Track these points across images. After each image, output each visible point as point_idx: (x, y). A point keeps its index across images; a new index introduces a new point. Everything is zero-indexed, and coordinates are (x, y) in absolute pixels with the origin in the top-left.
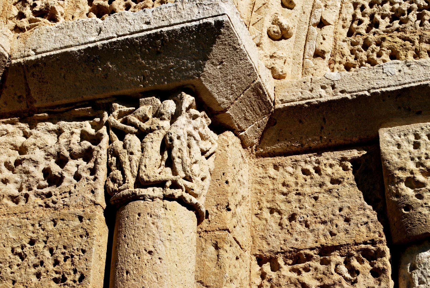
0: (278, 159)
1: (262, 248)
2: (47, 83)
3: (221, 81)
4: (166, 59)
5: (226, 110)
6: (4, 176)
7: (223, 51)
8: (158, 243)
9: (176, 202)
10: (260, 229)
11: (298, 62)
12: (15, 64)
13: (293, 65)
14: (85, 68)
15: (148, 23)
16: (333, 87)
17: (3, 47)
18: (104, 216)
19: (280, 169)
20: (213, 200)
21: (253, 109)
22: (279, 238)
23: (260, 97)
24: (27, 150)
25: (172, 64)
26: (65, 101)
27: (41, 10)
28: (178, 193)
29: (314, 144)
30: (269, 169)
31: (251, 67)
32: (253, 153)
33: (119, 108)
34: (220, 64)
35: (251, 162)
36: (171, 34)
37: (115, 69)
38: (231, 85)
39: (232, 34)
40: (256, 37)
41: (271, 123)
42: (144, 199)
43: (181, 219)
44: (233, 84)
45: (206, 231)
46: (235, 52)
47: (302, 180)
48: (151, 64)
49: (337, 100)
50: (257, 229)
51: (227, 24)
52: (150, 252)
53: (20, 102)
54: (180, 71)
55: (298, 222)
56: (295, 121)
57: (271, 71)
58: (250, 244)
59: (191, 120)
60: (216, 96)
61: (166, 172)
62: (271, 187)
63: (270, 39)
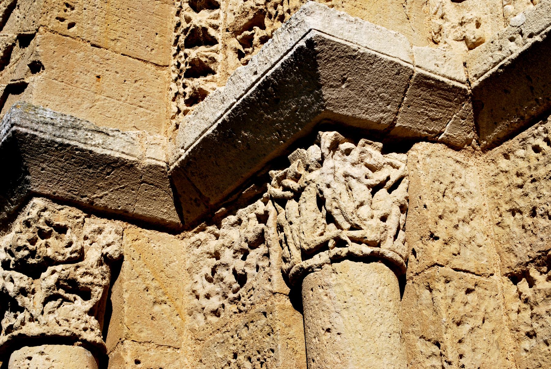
0: (505, 146)
1: (510, 264)
2: (208, 177)
3: (360, 99)
4: (287, 104)
5: (392, 124)
6: (206, 291)
7: (336, 67)
8: (334, 317)
9: (348, 261)
10: (505, 241)
11: (496, 15)
12: (173, 170)
13: (492, 21)
14: (227, 146)
15: (256, 73)
16: (521, 33)
17: (154, 159)
18: (291, 303)
19: (511, 157)
20: (416, 234)
21: (436, 104)
22: (524, 245)
23: (435, 87)
24: (219, 254)
25: (294, 106)
26: (231, 188)
27: (191, 97)
28: (344, 251)
29: (533, 111)
30: (500, 161)
31: (393, 64)
32: (477, 150)
33: (276, 174)
34: (343, 83)
35: (479, 161)
36: (276, 75)
37: (251, 136)
38: (379, 95)
39: (334, 45)
40: (438, 8)
41: (477, 108)
42: (313, 271)
43: (358, 278)
44: (381, 93)
45: (417, 274)
46: (355, 60)
47: (535, 161)
48: (277, 115)
49: (528, 49)
50: (502, 242)
51: (319, 38)
52: (328, 330)
53: (198, 205)
54: (304, 110)
55: (539, 216)
56: (500, 94)
57: (464, 43)
58: (498, 263)
59: (345, 157)
60: (364, 116)
61: (329, 229)
62: (506, 183)
63: (455, 3)
